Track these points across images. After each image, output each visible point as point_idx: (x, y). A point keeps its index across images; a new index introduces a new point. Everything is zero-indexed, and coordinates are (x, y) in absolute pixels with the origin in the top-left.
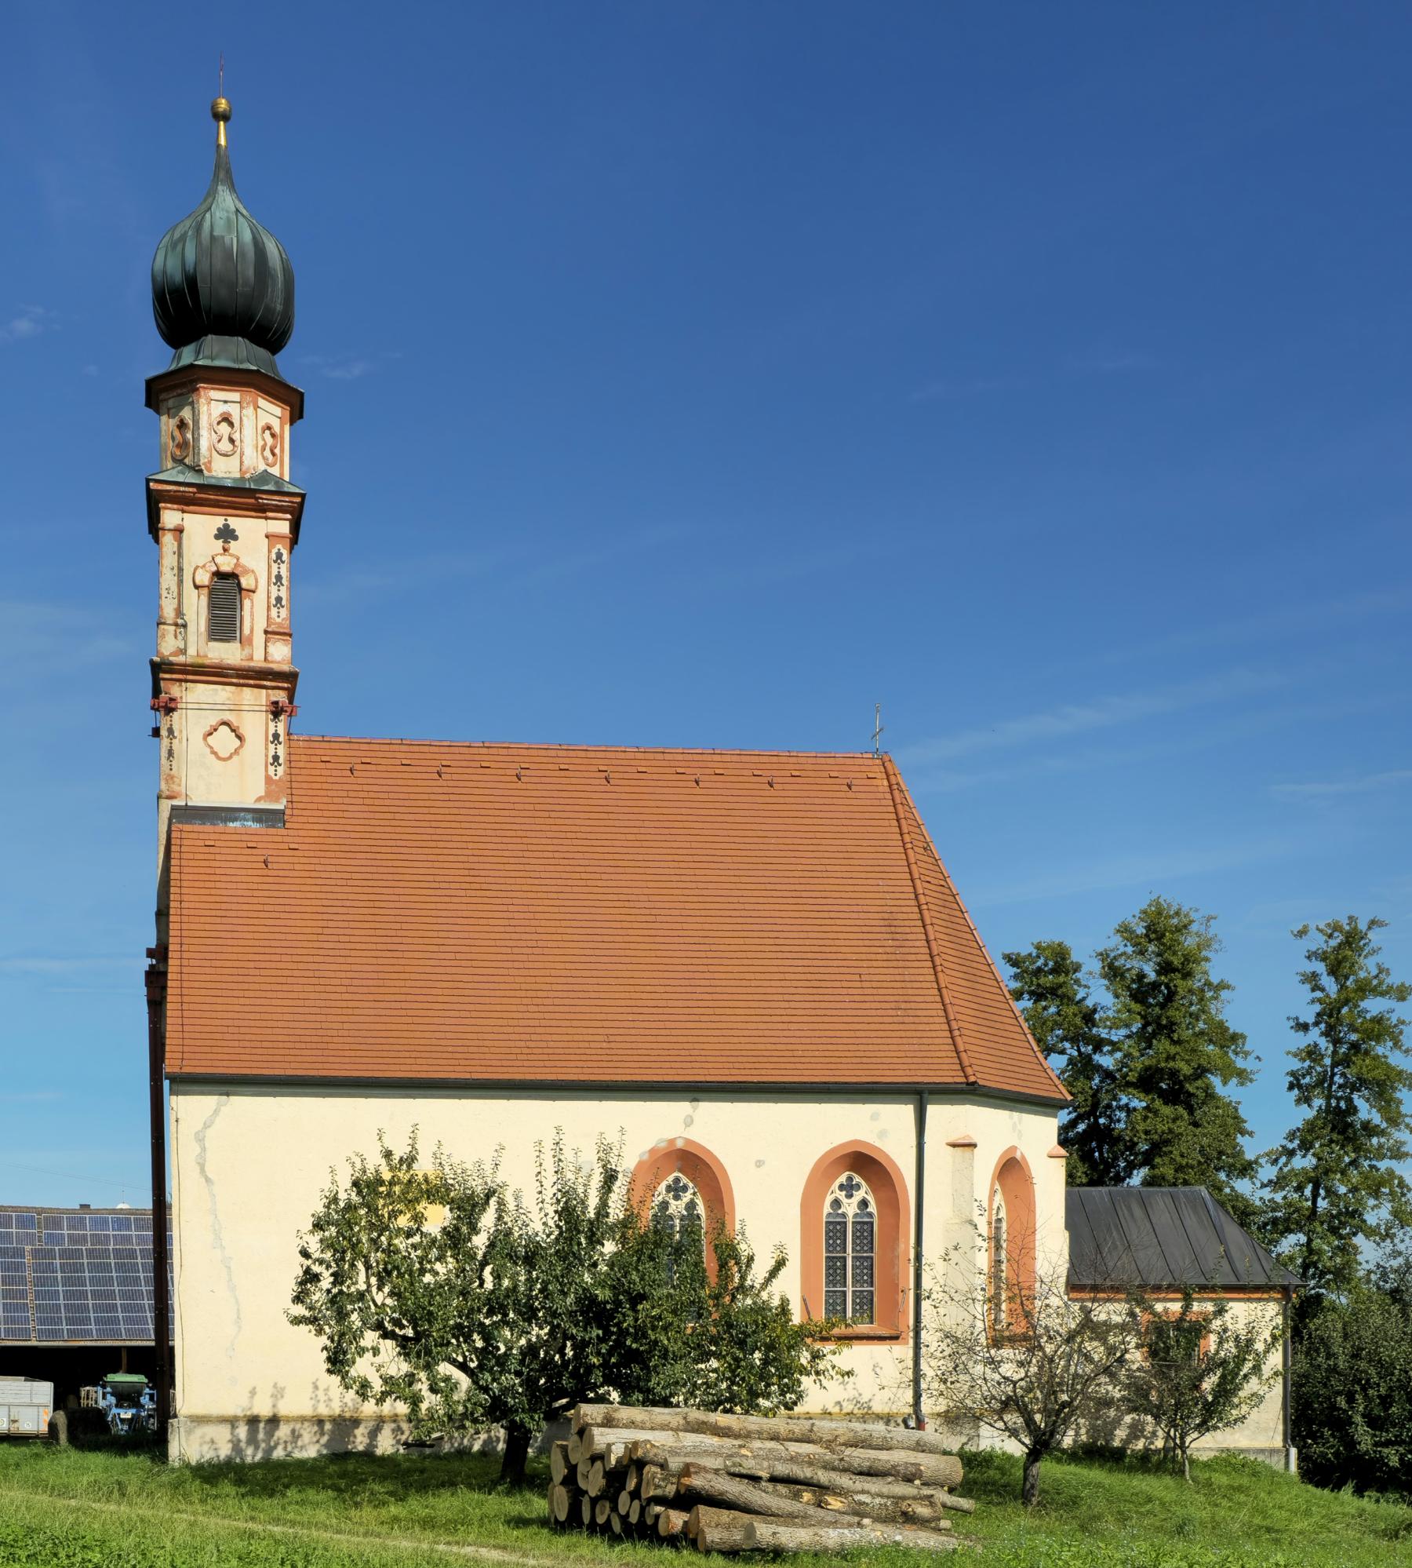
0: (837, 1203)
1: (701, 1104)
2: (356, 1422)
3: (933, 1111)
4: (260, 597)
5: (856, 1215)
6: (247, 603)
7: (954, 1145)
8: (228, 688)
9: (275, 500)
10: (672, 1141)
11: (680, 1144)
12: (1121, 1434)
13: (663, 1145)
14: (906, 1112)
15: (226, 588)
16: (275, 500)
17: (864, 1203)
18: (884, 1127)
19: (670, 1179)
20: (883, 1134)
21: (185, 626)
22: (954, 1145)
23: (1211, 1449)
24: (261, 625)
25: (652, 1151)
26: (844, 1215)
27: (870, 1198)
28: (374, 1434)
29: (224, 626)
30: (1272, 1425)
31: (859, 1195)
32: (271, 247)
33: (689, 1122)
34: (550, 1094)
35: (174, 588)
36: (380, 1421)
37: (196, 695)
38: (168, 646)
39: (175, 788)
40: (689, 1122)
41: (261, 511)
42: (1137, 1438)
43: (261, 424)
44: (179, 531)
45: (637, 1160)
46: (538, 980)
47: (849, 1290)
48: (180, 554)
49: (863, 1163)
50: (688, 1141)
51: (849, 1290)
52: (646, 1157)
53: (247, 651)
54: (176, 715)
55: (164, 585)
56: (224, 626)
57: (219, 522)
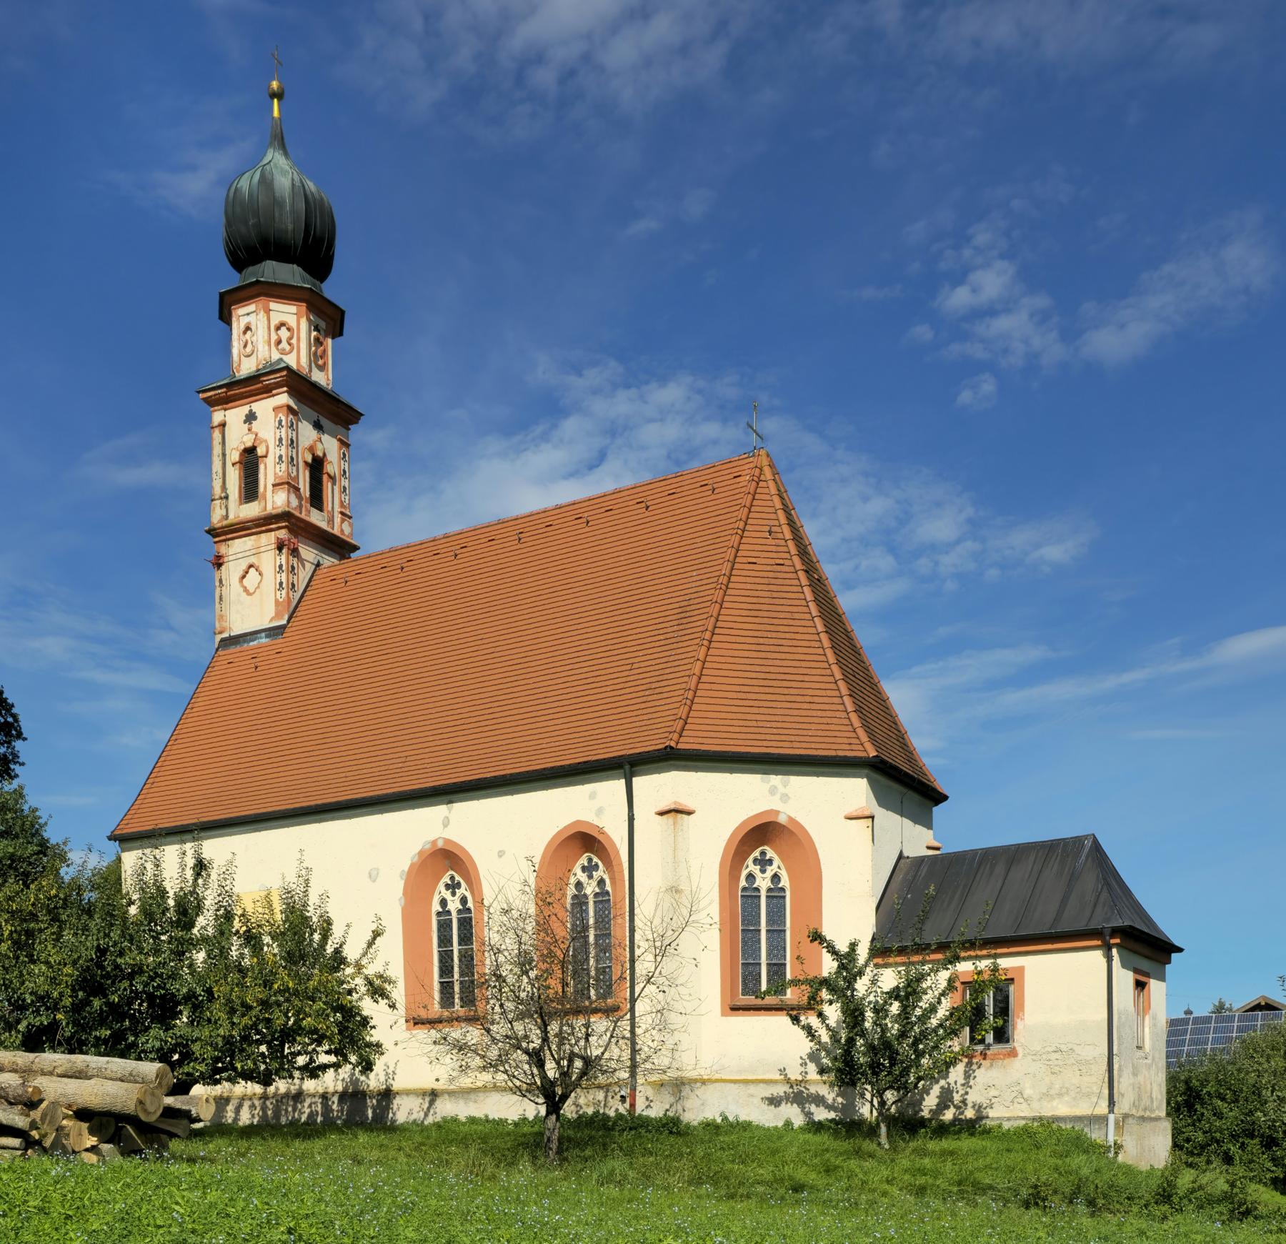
0: (751, 877)
1: (455, 805)
2: (227, 1100)
3: (641, 783)
4: (270, 460)
5: (769, 890)
6: (262, 467)
7: (662, 814)
8: (252, 537)
9: (271, 380)
10: (434, 842)
11: (440, 844)
12: (931, 1101)
13: (428, 846)
14: (616, 786)
15: (250, 460)
16: (271, 380)
17: (776, 878)
18: (596, 804)
19: (446, 879)
20: (600, 811)
21: (227, 498)
22: (662, 814)
23: (1023, 1118)
24: (271, 480)
25: (420, 853)
26: (757, 889)
27: (606, 877)
28: (238, 1110)
29: (250, 491)
30: (1095, 1089)
31: (770, 871)
32: (311, 186)
33: (446, 823)
34: (346, 813)
35: (220, 471)
36: (243, 1098)
37: (238, 549)
38: (216, 517)
39: (224, 624)
40: (446, 823)
41: (268, 391)
42: (947, 1107)
43: (274, 322)
44: (223, 425)
45: (409, 863)
46: (754, 724)
47: (456, 976)
48: (223, 442)
49: (585, 841)
50: (447, 841)
51: (456, 976)
52: (416, 859)
53: (263, 504)
54: (223, 568)
55: (214, 470)
56: (250, 491)
57: (246, 409)
